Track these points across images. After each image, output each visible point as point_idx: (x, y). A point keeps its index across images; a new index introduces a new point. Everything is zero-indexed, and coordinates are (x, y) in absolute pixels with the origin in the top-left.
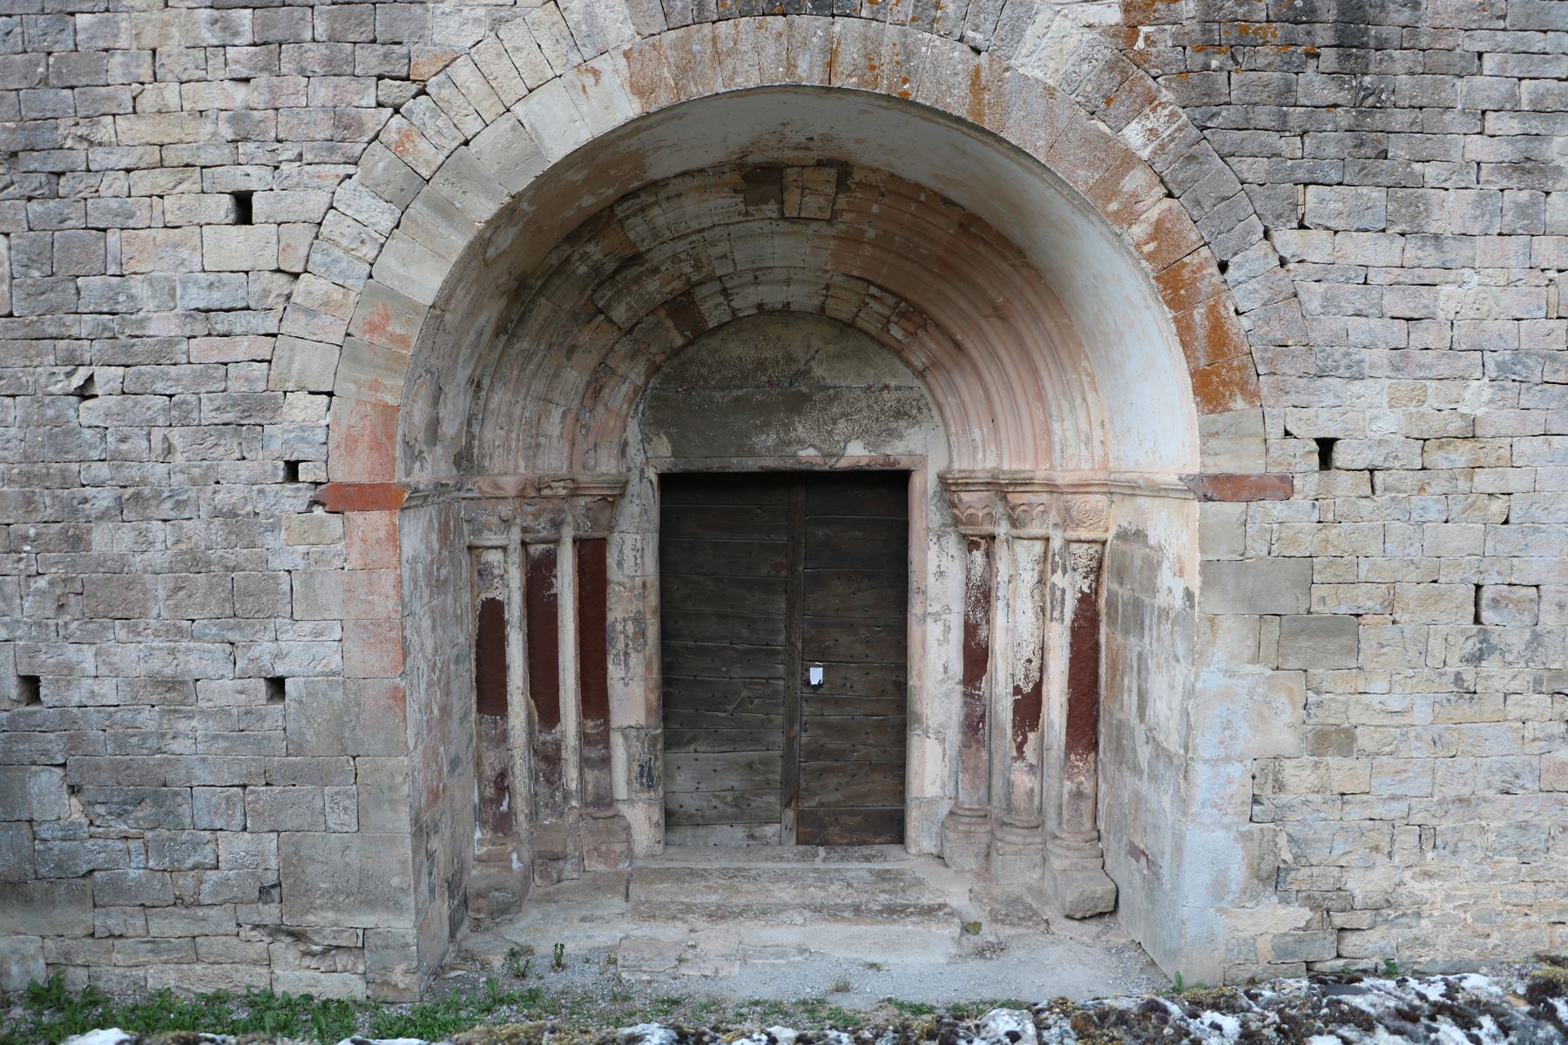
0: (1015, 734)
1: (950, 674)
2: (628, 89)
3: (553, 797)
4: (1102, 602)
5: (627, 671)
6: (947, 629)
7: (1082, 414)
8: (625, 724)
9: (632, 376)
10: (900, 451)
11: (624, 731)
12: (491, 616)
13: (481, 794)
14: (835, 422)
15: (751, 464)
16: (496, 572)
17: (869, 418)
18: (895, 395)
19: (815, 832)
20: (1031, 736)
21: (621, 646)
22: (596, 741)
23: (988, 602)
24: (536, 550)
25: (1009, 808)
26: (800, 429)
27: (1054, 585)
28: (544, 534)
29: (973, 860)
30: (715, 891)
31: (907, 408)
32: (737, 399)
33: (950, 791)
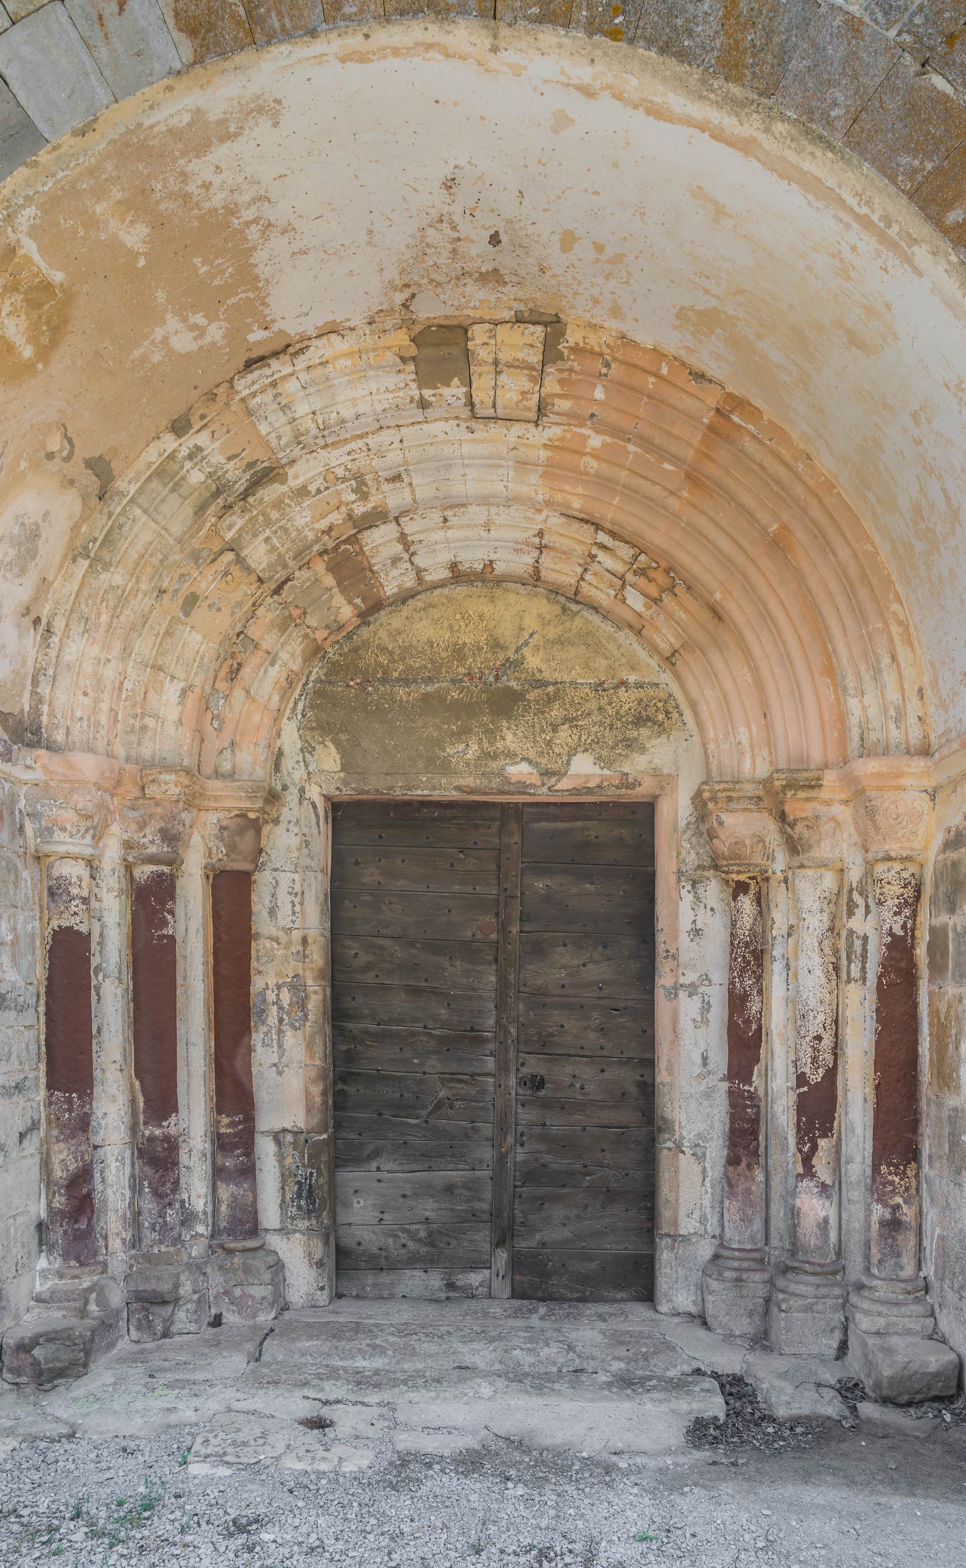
0: (800, 1142)
1: (711, 1066)
2: (171, 22)
3: (162, 1215)
4: (921, 952)
5: (281, 1056)
6: (706, 1007)
7: (890, 678)
8: (277, 1126)
9: (284, 656)
11: (277, 1136)
12: (68, 957)
13: (49, 1205)
14: (555, 729)
15: (444, 789)
16: (75, 891)
17: (601, 724)
18: (634, 694)
19: (540, 1283)
20: (823, 1143)
21: (272, 1020)
22: (235, 1146)
23: (760, 965)
24: (144, 872)
25: (795, 1248)
26: (509, 737)
27: (851, 932)
28: (152, 850)
29: (745, 1321)
30: (382, 1351)
32: (426, 697)
33: (712, 1226)
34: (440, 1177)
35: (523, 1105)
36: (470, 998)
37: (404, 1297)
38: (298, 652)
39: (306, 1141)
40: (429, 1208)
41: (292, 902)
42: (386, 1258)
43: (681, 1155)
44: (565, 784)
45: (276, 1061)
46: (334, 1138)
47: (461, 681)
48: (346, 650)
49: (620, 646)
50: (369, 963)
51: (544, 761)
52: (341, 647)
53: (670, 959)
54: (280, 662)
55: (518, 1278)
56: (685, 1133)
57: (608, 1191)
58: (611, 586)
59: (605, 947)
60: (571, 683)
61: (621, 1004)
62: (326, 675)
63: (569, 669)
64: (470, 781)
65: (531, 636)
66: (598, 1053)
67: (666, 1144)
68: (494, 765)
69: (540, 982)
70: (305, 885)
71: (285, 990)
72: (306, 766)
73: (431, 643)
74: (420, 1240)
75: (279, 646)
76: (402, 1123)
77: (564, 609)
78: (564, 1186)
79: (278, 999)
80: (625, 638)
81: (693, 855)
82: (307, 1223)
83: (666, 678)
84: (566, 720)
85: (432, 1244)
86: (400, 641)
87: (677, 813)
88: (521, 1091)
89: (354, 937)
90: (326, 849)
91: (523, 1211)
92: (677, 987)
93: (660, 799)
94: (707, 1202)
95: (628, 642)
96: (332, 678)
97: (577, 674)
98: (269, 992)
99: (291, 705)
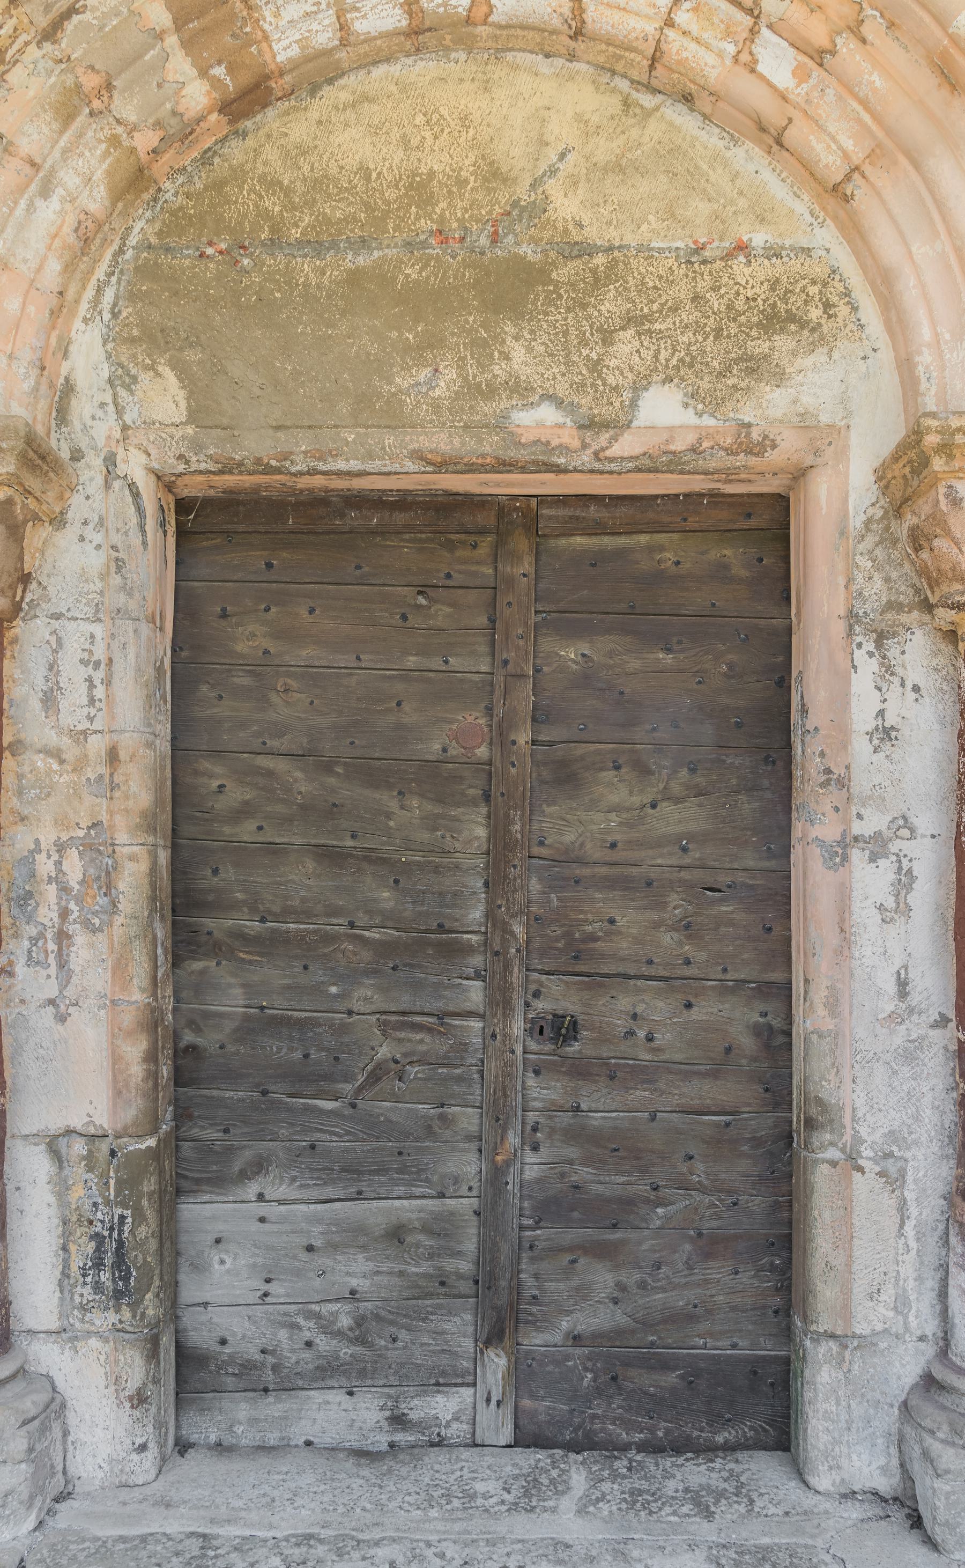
1: (915, 998)
5: (65, 983)
6: (905, 880)
8: (56, 1124)
9: (69, 179)
10: (776, 413)
11: (54, 1145)
14: (607, 337)
17: (698, 328)
18: (763, 269)
21: (48, 914)
26: (518, 354)
31: (797, 301)
32: (355, 278)
34: (375, 1212)
35: (537, 1073)
36: (436, 869)
37: (308, 1444)
38: (99, 174)
39: (113, 1153)
40: (357, 1271)
41: (90, 680)
42: (275, 1368)
43: (857, 1176)
44: (627, 446)
45: (53, 992)
46: (176, 1138)
47: (424, 245)
48: (199, 185)
49: (735, 176)
50: (246, 803)
51: (586, 401)
52: (190, 181)
53: (832, 787)
54: (60, 191)
55: (526, 1403)
56: (863, 1131)
57: (700, 1235)
58: (728, 34)
59: (693, 771)
60: (640, 248)
61: (723, 879)
62: (159, 234)
63: (638, 220)
64: (442, 442)
65: (562, 156)
66: (679, 972)
67: (825, 1152)
68: (488, 409)
69: (569, 837)
70: (115, 645)
71: (73, 854)
72: (120, 412)
73: (365, 172)
74: (340, 1334)
75: (57, 154)
76: (307, 1109)
77: (627, 103)
78: (615, 1226)
79: (60, 871)
80: (749, 159)
81: (878, 583)
82: (112, 1317)
83: (825, 236)
84: (631, 320)
85: (361, 1340)
86: (306, 168)
87: (845, 500)
88: (533, 1046)
89: (217, 753)
90: (160, 580)
91: (536, 1276)
92: (847, 842)
93: (812, 475)
94: (908, 1270)
95: (752, 168)
96: (171, 241)
97: (651, 231)
98: (41, 858)
99: (90, 293)
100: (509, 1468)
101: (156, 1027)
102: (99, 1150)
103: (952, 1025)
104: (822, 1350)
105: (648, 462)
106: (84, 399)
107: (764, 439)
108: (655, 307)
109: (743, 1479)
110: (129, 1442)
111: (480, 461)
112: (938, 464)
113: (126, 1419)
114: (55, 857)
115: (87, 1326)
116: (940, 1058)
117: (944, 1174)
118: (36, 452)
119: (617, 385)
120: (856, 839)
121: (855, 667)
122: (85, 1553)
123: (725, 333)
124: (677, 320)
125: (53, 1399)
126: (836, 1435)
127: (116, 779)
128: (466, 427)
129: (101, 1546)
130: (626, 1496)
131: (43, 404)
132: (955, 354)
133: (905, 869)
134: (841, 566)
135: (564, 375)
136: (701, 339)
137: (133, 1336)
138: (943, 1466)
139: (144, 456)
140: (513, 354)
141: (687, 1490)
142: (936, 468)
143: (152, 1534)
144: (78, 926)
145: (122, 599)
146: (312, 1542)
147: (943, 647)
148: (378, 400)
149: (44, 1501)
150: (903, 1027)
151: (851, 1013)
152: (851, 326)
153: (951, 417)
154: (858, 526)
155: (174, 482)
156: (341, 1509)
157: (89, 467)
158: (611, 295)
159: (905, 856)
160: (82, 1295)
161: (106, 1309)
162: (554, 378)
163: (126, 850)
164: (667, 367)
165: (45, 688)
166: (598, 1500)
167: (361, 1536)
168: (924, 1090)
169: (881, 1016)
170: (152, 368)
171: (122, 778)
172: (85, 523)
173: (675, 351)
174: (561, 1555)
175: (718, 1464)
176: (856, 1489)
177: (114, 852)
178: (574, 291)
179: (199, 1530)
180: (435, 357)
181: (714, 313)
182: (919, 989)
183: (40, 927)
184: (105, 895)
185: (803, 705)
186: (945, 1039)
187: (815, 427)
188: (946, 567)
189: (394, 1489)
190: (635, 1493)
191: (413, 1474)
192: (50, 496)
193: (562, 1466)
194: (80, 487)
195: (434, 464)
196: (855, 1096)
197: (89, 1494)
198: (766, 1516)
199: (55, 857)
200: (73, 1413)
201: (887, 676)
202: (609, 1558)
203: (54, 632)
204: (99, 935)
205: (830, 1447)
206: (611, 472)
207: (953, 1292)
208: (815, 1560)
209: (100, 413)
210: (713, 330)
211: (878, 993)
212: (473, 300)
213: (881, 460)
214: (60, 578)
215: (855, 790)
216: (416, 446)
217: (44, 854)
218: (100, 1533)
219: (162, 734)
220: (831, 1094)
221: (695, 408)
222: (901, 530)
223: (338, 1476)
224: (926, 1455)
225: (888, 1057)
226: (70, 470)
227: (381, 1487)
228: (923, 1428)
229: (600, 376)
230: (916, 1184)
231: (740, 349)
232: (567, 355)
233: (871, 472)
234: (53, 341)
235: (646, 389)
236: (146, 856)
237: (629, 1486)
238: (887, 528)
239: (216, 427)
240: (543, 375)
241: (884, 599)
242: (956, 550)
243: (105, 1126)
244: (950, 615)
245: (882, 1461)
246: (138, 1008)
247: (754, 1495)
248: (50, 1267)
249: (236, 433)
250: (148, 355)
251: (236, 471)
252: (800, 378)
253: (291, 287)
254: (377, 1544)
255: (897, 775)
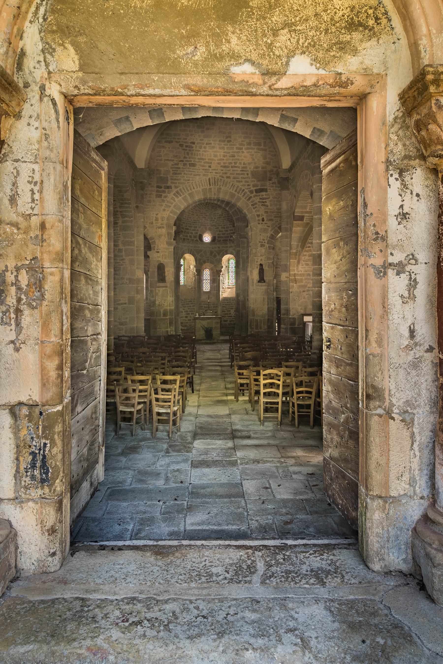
1: (418, 339)
6: (413, 284)
8: (14, 399)
10: (353, 68)
17: (317, 29)
26: (234, 40)
39: (41, 413)
41: (32, 190)
43: (391, 421)
44: (284, 83)
51: (265, 62)
53: (379, 241)
56: (394, 401)
68: (220, 66)
70: (44, 174)
71: (24, 272)
72: (47, 65)
79: (17, 280)
81: (400, 146)
82: (40, 492)
84: (286, 25)
90: (66, 145)
92: (386, 266)
93: (370, 97)
94: (415, 465)
98: (8, 274)
99: (33, 9)
100: (228, 560)
101: (62, 353)
102: (34, 412)
103: (436, 350)
104: (375, 504)
105: (294, 91)
106: (30, 59)
107: (347, 80)
108: (298, 19)
109: (338, 564)
110: (47, 551)
111: (216, 90)
112: (432, 89)
113: (46, 541)
114: (15, 273)
115: (27, 496)
116: (430, 366)
117: (432, 421)
118: (6, 81)
119: (280, 55)
120: (390, 264)
121: (389, 185)
122: (24, 610)
123: (330, 31)
124: (308, 25)
125: (11, 532)
126: (382, 544)
127: (45, 237)
128: (210, 74)
129: (32, 606)
130: (284, 574)
131: (10, 61)
132: (438, 40)
133: (413, 278)
134: (383, 139)
135: (255, 50)
136: (318, 34)
137: (50, 501)
138: (437, 562)
139: (59, 86)
140: (232, 40)
141: (312, 571)
142: (431, 91)
143: (57, 599)
144: (25, 306)
145: (48, 153)
146: (135, 602)
147: (430, 176)
148: (168, 61)
149: (5, 583)
150: (413, 352)
151: (388, 346)
152: (388, 28)
153: (439, 66)
154: (391, 120)
155: (73, 99)
156: (149, 583)
157: (32, 91)
158: (277, 13)
159: (413, 272)
160: (25, 481)
161: (37, 488)
162: (251, 52)
163: (49, 270)
164: (303, 47)
165: (11, 194)
166: (271, 577)
167: (158, 598)
168: (422, 381)
169: (402, 347)
170: (62, 45)
171: (47, 236)
172: (30, 117)
173: (306, 39)
174: (255, 607)
175: (325, 556)
176: (392, 569)
177: (43, 271)
178: (260, 11)
179: (80, 596)
180: (195, 41)
181: (324, 22)
182: (420, 334)
183: (7, 307)
184: (39, 291)
185: (365, 203)
186: (429, 358)
187: (371, 75)
188: (434, 138)
189: (174, 572)
190: (288, 572)
191: (182, 564)
192: (13, 104)
193: (252, 558)
194: (28, 100)
195: (194, 91)
196: (390, 384)
197: (27, 577)
198: (350, 584)
199: (15, 273)
200: (20, 538)
201: (404, 189)
202: (278, 608)
203: (15, 168)
204: (36, 310)
205: (379, 550)
206: (276, 96)
207: (438, 477)
208: (376, 608)
209: (37, 66)
210: (324, 30)
211: (401, 336)
212: (213, 15)
213: (402, 90)
214: (19, 143)
215: (390, 242)
216: (186, 82)
217: (9, 273)
218: (32, 599)
219: (67, 216)
220: (379, 383)
221: (316, 66)
222: (412, 122)
223: (146, 565)
224: (427, 555)
225: (405, 366)
226: (23, 92)
227: (167, 571)
228: (426, 542)
229: (272, 51)
230: (419, 425)
231: (336, 38)
232: (257, 41)
233: (397, 95)
234: (15, 30)
235: (293, 57)
236: (58, 273)
237: (285, 569)
238: (404, 121)
239: (93, 73)
240: (245, 50)
241: (403, 154)
242: (439, 130)
243: (37, 401)
244: (435, 160)
245: (404, 556)
246: (54, 345)
247: (344, 573)
248: (10, 468)
249: (102, 76)
250: (61, 39)
251: (102, 94)
252: (364, 52)
253: (128, 8)
254: (166, 602)
255: (409, 235)
